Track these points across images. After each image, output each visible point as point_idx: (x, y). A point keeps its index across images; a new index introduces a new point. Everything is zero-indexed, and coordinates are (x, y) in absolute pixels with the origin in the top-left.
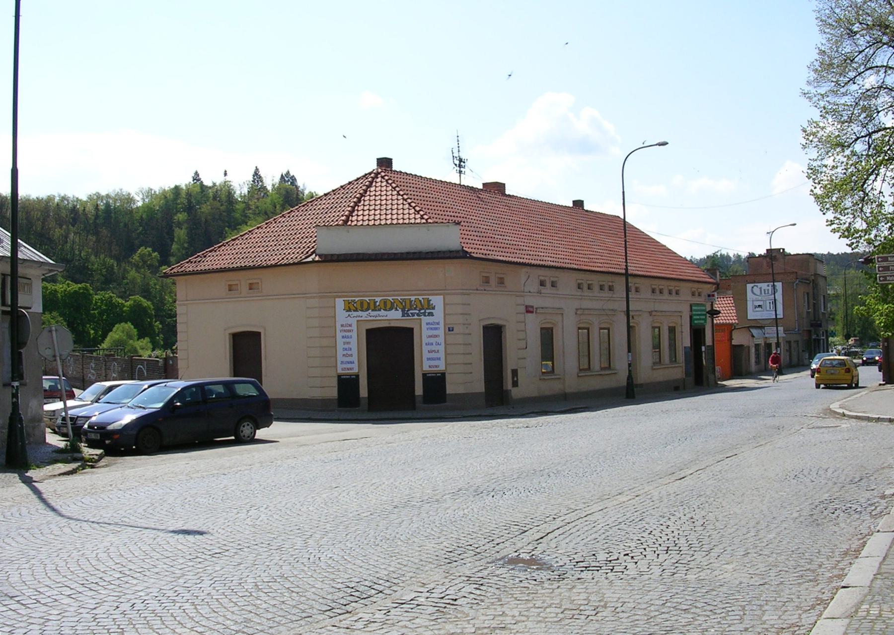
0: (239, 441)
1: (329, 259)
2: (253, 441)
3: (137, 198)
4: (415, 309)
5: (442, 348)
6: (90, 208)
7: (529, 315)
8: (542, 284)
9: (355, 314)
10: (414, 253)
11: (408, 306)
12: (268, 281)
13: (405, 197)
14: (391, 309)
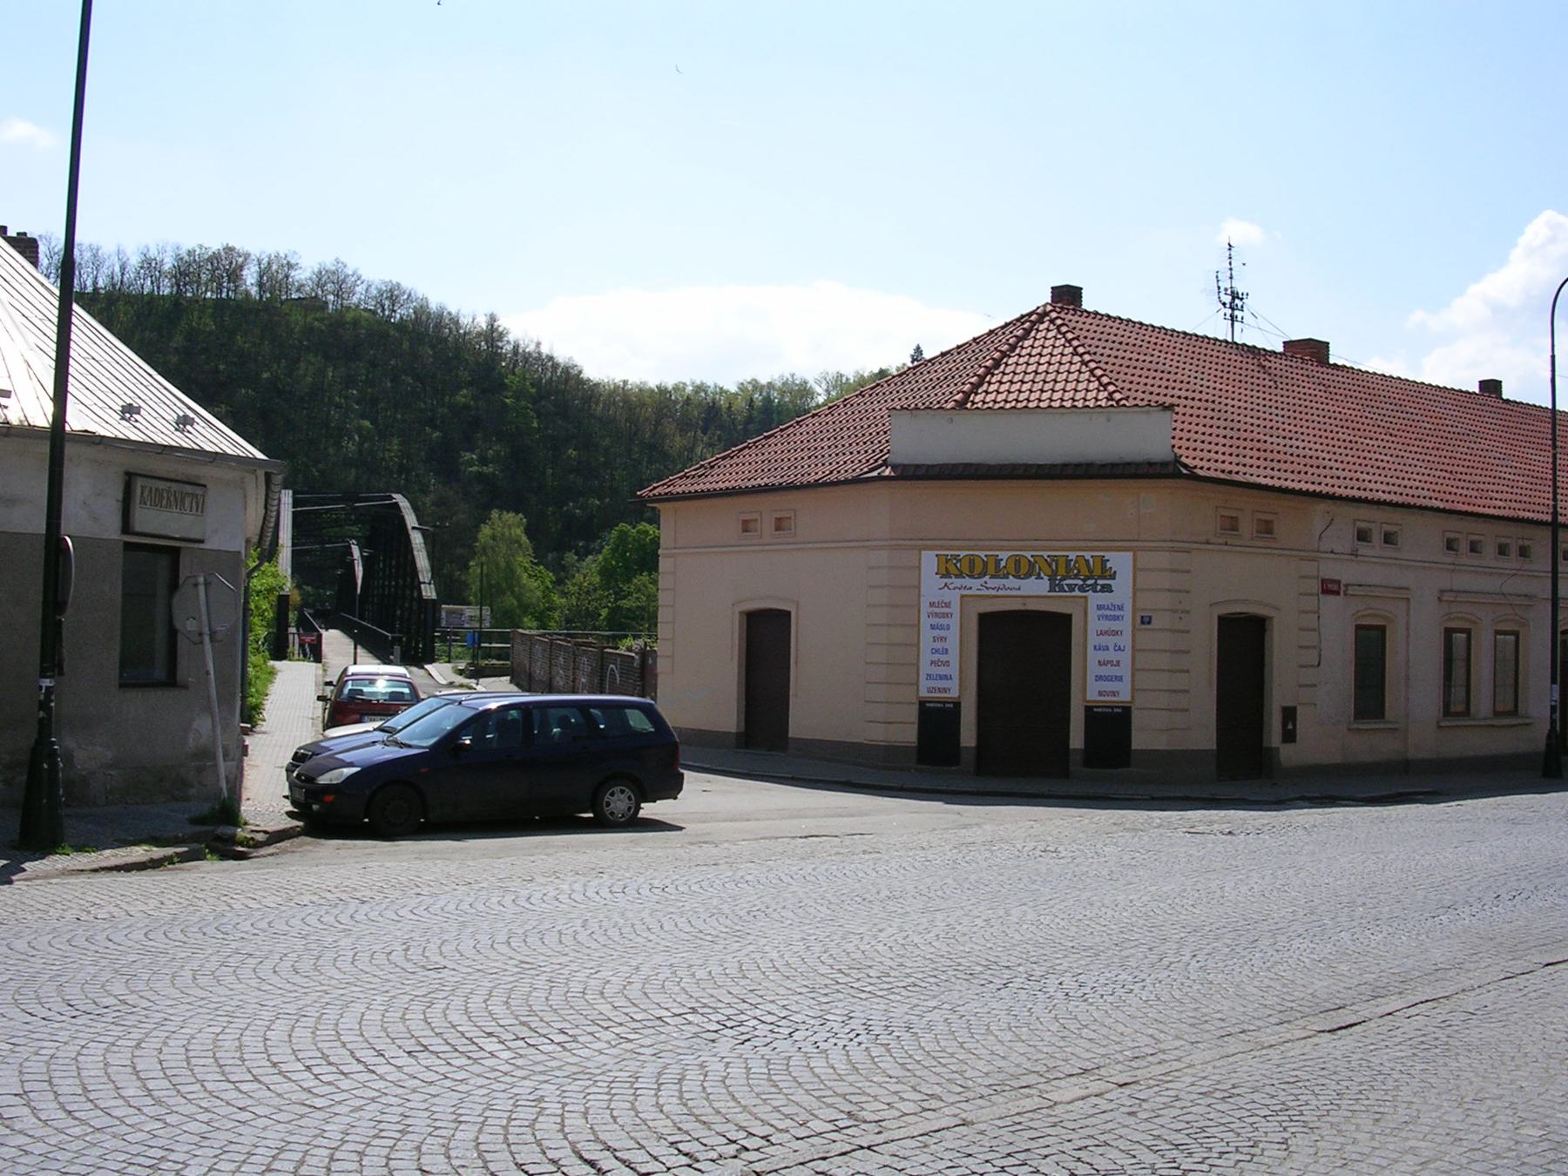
0: (603, 824)
1: (910, 474)
2: (635, 824)
3: (818, 390)
4: (1076, 577)
5: (1125, 658)
6: (741, 404)
7: (1331, 598)
8: (1363, 536)
9: (958, 582)
10: (1078, 465)
11: (1062, 571)
12: (810, 516)
13: (1087, 357)
14: (1028, 576)
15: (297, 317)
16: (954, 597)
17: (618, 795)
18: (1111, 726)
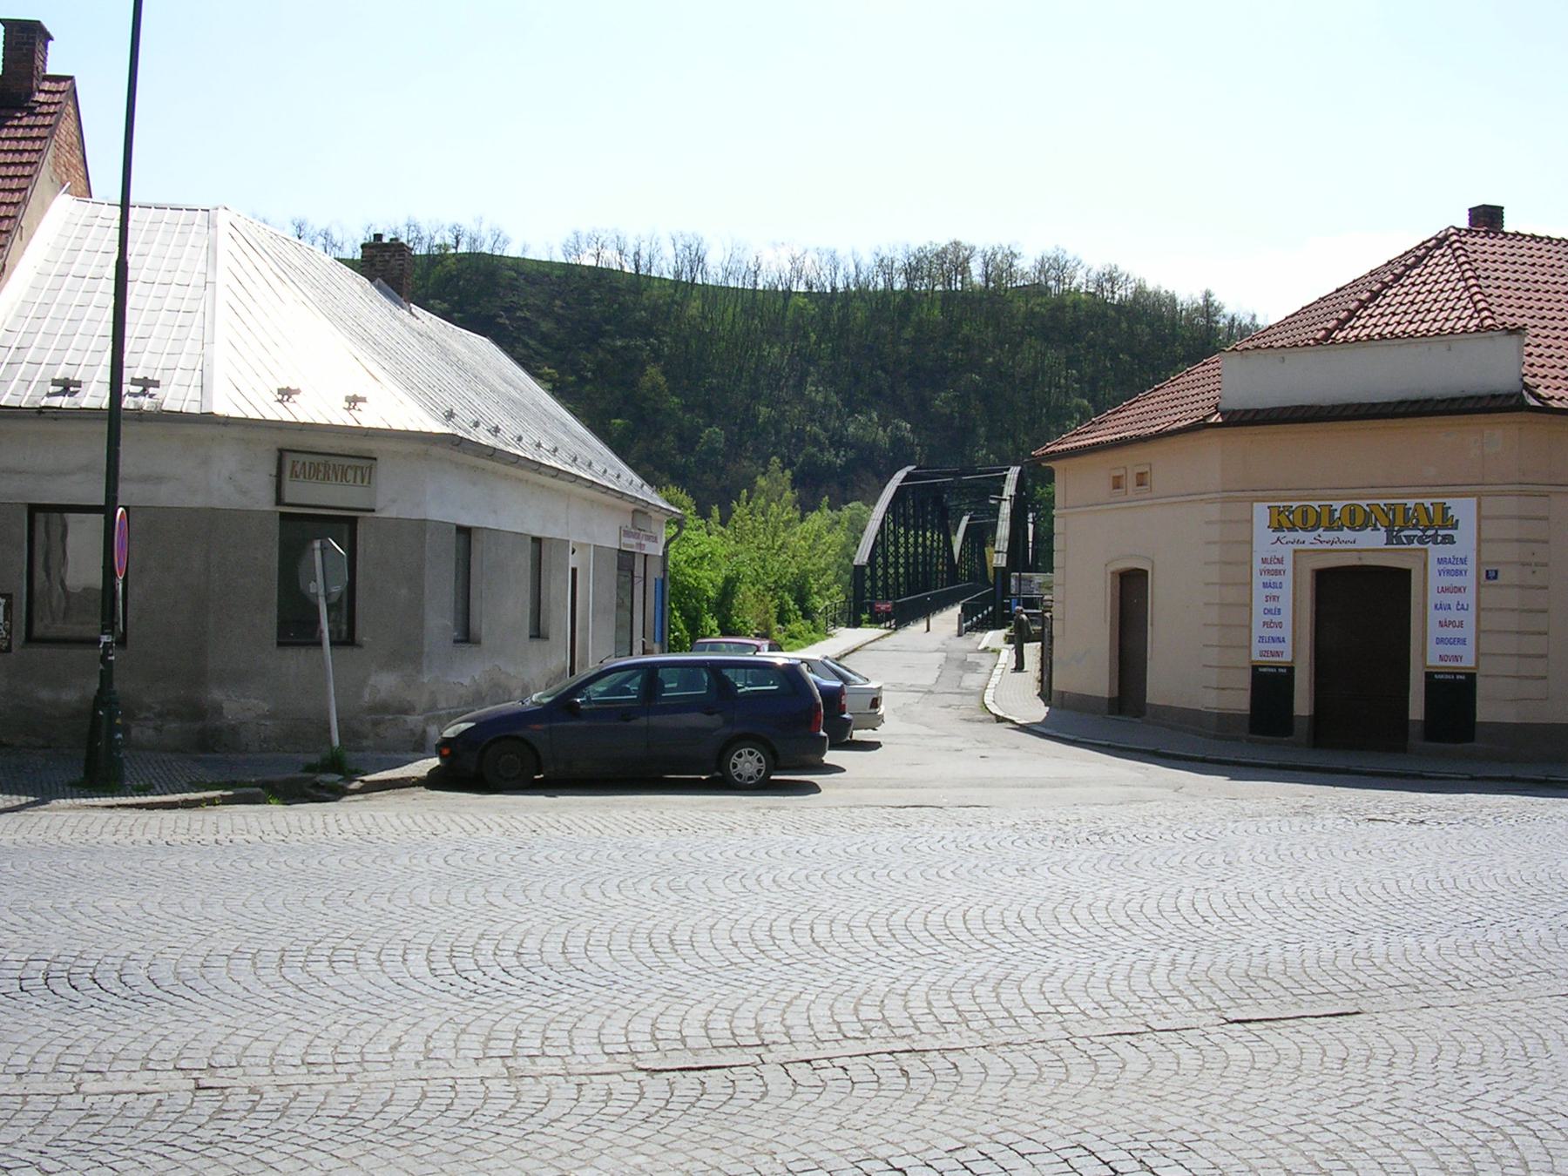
4: (1415, 527)
5: (1469, 618)
11: (1400, 521)
14: (1363, 527)
15: (1020, 305)
16: (1286, 552)
17: (746, 757)
18: (1452, 694)
